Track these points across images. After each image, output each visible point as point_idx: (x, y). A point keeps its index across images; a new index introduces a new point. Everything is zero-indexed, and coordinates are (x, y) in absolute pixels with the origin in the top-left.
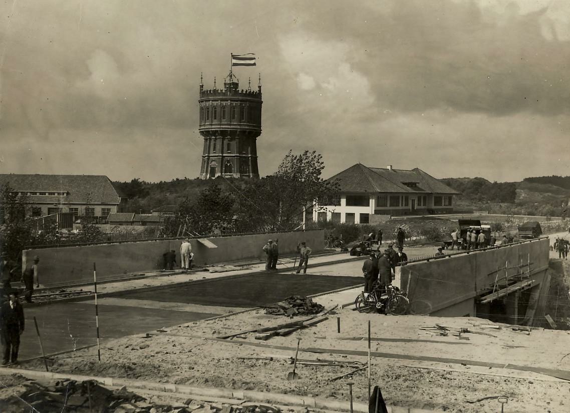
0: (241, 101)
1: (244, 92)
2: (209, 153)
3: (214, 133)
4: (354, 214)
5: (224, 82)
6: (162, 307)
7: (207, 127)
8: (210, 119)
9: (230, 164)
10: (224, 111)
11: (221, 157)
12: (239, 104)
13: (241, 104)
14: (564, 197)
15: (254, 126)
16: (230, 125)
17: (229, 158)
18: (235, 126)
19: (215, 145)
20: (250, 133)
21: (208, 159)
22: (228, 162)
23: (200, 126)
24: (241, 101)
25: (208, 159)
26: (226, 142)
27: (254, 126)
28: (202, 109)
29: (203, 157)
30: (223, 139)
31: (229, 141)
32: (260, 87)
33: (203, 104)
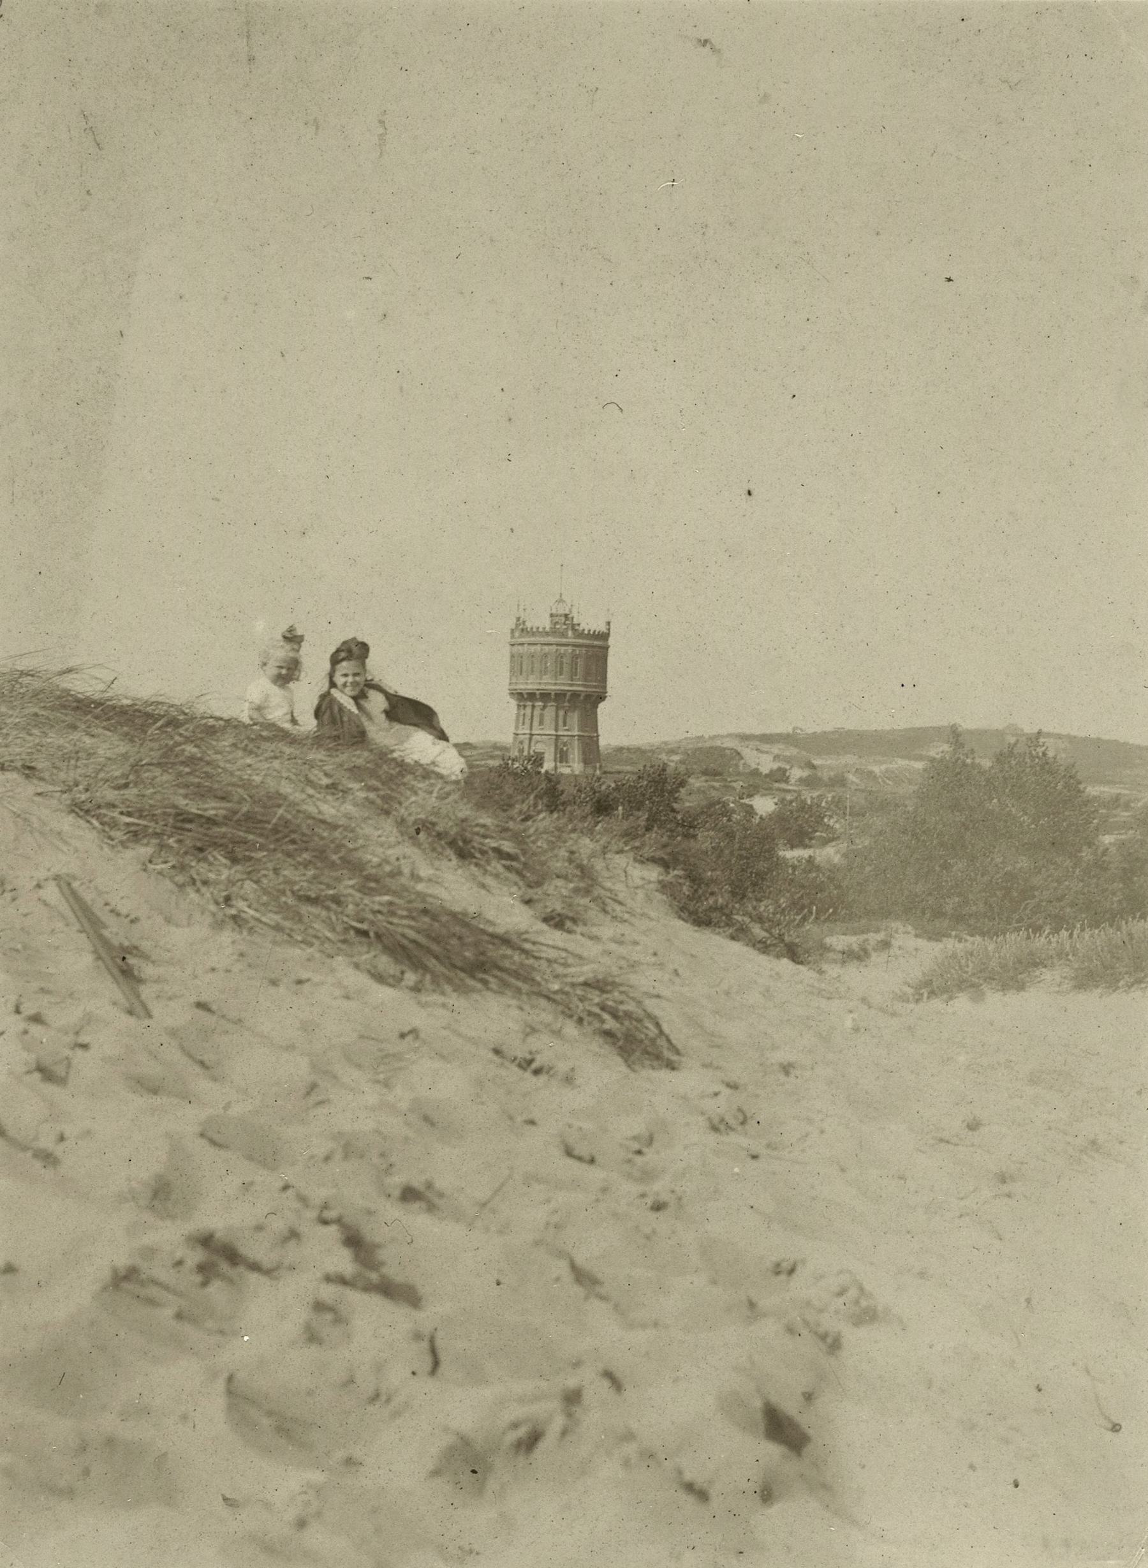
0: (574, 645)
1: (591, 632)
2: (531, 729)
3: (531, 696)
4: (1041, 730)
5: (550, 612)
6: (519, 991)
7: (530, 684)
8: (524, 674)
9: (568, 749)
10: (562, 663)
11: (528, 736)
12: (570, 651)
13: (573, 650)
14: (1129, 816)
15: (595, 687)
16: (571, 685)
17: (565, 739)
18: (561, 684)
19: (542, 716)
20: (588, 696)
21: (530, 739)
22: (565, 744)
23: (510, 684)
24: (574, 645)
25: (530, 739)
26: (561, 713)
27: (595, 687)
28: (512, 656)
29: (515, 734)
30: (557, 709)
31: (541, 709)
32: (609, 623)
33: (516, 648)
